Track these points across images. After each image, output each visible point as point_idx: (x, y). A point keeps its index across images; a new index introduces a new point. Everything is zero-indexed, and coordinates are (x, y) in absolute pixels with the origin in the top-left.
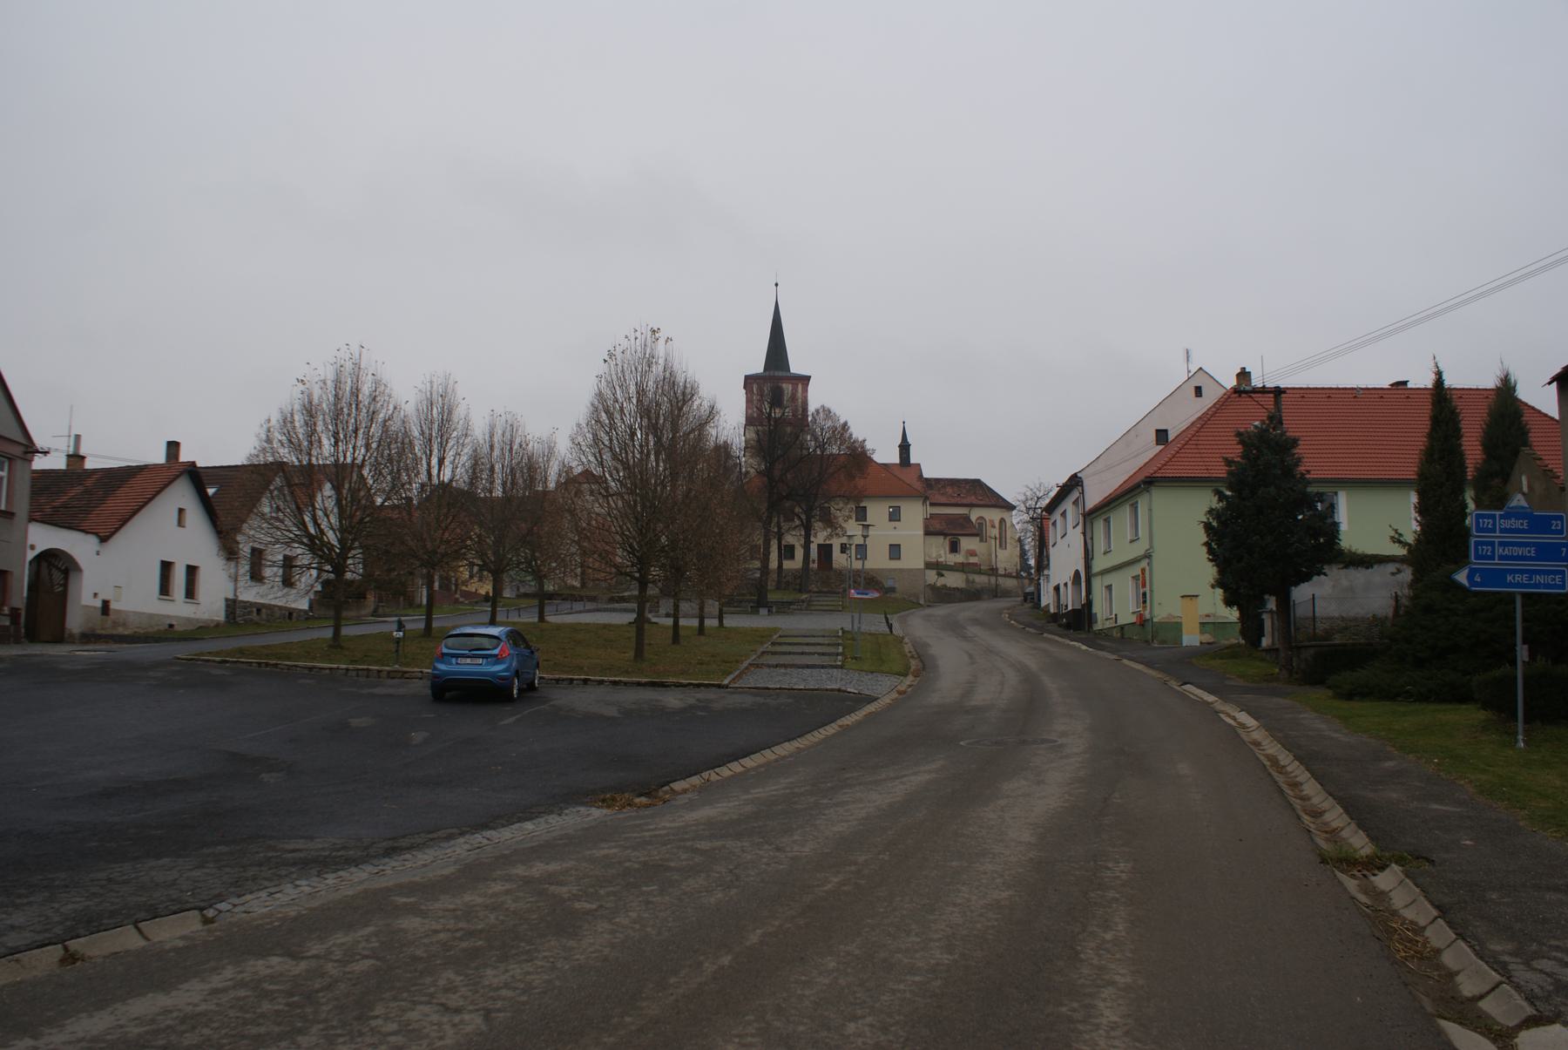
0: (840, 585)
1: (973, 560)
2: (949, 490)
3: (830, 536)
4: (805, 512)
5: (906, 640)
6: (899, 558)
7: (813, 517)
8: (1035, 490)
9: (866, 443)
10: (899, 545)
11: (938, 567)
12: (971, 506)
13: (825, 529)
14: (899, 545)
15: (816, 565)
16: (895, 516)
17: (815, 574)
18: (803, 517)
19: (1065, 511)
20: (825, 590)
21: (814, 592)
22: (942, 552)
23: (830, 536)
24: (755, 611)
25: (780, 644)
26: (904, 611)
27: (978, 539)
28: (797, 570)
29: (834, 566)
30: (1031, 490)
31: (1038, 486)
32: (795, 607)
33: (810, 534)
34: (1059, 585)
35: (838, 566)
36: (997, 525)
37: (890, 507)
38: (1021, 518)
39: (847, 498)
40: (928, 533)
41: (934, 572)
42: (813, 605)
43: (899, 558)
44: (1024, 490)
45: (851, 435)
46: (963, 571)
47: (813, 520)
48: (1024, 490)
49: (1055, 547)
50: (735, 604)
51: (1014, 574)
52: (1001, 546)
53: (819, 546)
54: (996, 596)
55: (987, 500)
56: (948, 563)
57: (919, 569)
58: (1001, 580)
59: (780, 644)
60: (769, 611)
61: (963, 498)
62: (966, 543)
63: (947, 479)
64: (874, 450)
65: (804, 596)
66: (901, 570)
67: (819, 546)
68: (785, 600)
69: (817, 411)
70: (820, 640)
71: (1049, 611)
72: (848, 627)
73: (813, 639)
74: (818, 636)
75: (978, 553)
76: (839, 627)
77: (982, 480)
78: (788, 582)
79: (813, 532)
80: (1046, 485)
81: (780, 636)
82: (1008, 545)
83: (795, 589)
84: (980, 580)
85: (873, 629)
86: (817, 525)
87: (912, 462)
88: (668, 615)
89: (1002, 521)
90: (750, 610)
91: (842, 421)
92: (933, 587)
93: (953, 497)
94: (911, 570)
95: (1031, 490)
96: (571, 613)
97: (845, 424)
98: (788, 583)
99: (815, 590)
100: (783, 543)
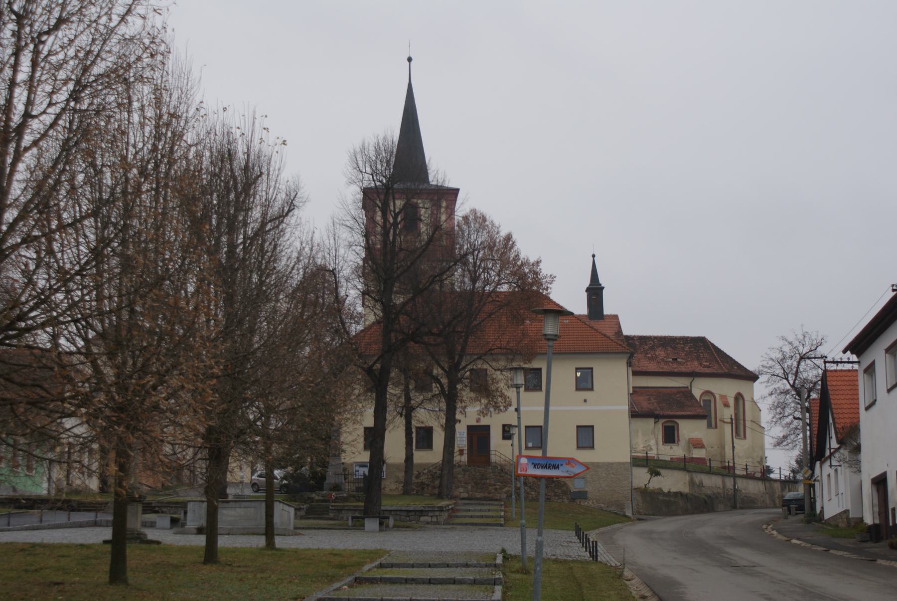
0: (501, 488)
1: (698, 453)
2: (661, 353)
3: (483, 413)
4: (448, 374)
5: (627, 573)
6: (592, 447)
7: (460, 381)
8: (796, 343)
9: (541, 266)
10: (592, 427)
11: (654, 466)
12: (693, 375)
13: (477, 399)
14: (592, 427)
15: (464, 458)
16: (585, 383)
17: (464, 471)
18: (444, 381)
19: (873, 363)
20: (478, 495)
21: (463, 499)
22: (652, 443)
23: (483, 413)
24: (358, 524)
25: (372, 581)
26: (603, 526)
27: (705, 422)
28: (435, 465)
29: (493, 458)
30: (790, 343)
31: (801, 337)
32: (428, 519)
33: (455, 408)
34: (885, 474)
35: (498, 459)
36: (731, 402)
37: (577, 369)
38: (776, 386)
39: (511, 353)
40: (634, 414)
41: (645, 470)
42: (457, 517)
43: (592, 447)
44: (781, 343)
45: (517, 256)
46: (684, 469)
47: (459, 386)
48: (781, 343)
49: (874, 409)
50: (331, 515)
51: (758, 475)
52: (736, 433)
53: (470, 428)
54: (734, 507)
55: (716, 366)
56: (661, 458)
57: (623, 463)
58: (741, 484)
59: (372, 581)
60: (381, 524)
61: (680, 363)
62: (688, 429)
63: (656, 338)
64: (553, 278)
65: (444, 503)
66: (597, 465)
67: (470, 428)
68: (411, 509)
69: (466, 218)
70: (457, 574)
71: (861, 520)
72: (514, 548)
73: (410, 570)
74: (457, 566)
75: (705, 443)
76: (499, 548)
77: (707, 337)
78: (423, 483)
79: (459, 405)
80: (814, 337)
81: (381, 566)
82: (748, 431)
83: (431, 495)
84: (711, 482)
85: (560, 552)
86: (466, 394)
87: (605, 313)
88: (200, 531)
89: (739, 397)
90: (350, 522)
91: (503, 233)
92: (645, 493)
93: (666, 363)
94: (610, 465)
95: (790, 343)
96: (38, 529)
97: (509, 238)
98: (422, 485)
99: (465, 495)
100: (414, 423)
